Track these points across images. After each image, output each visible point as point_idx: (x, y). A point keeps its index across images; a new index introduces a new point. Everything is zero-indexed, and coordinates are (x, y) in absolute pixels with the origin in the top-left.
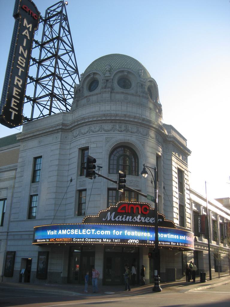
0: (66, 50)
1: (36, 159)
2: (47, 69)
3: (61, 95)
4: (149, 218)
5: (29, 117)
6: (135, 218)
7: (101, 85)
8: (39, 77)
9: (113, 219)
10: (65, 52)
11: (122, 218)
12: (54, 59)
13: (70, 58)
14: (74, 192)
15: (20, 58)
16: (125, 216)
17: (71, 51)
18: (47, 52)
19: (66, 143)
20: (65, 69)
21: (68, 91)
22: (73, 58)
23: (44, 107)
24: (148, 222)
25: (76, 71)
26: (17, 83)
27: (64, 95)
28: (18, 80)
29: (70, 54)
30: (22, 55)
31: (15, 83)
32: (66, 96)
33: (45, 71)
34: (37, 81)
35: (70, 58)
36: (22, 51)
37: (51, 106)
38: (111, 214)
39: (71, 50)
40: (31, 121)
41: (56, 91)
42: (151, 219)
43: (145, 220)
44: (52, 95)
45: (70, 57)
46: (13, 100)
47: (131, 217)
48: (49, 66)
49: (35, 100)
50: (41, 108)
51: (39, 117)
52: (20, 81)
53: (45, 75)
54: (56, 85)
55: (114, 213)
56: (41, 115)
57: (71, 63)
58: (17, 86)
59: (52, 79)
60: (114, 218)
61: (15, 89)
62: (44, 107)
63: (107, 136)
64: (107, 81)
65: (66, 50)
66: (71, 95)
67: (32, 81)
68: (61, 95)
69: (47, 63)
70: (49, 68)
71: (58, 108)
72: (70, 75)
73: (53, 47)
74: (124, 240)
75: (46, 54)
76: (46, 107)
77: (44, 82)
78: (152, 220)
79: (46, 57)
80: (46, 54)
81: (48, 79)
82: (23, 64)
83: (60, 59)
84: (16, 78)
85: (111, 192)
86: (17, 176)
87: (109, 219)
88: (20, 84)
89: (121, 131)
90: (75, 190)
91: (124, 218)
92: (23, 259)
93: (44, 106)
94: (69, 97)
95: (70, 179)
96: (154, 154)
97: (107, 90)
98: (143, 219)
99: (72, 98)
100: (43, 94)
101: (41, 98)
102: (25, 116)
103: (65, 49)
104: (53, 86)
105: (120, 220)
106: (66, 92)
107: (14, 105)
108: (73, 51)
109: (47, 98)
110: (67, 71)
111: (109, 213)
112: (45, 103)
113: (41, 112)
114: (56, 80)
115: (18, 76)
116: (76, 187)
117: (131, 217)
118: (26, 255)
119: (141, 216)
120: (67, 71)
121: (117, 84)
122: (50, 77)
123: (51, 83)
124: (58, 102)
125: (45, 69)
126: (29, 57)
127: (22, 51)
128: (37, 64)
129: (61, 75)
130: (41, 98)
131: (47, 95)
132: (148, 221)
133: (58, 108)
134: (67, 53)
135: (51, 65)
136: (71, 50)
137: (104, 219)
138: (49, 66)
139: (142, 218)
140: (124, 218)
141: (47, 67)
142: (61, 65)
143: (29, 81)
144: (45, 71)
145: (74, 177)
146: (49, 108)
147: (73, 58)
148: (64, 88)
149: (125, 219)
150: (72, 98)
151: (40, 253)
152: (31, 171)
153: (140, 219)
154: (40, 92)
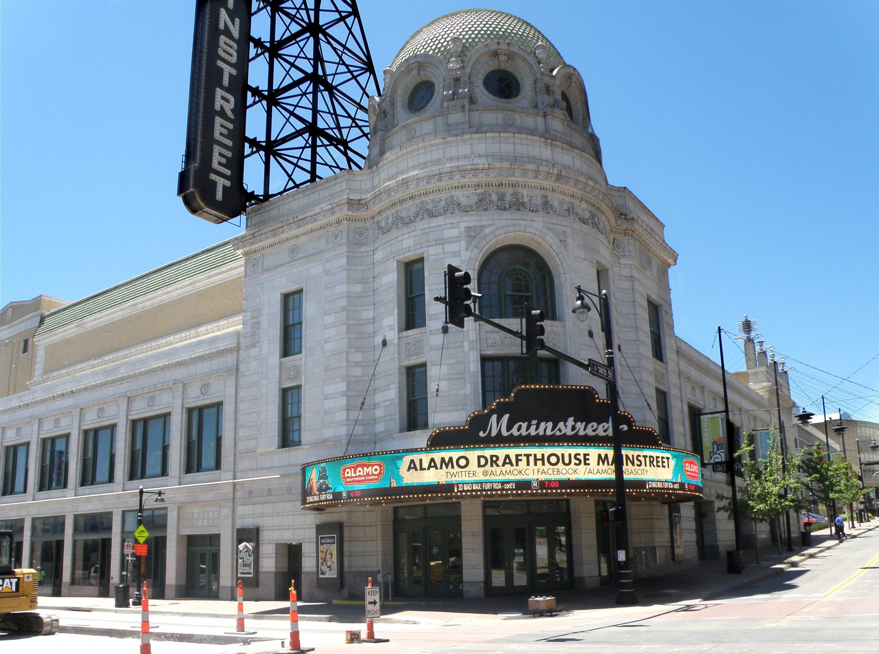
0: (340, 12)
1: (286, 297)
2: (292, 65)
3: (332, 129)
4: (595, 424)
5: (260, 191)
6: (561, 425)
7: (442, 92)
8: (275, 87)
9: (505, 433)
10: (336, 16)
11: (528, 428)
12: (308, 38)
13: (351, 32)
14: (396, 371)
15: (223, 39)
16: (534, 422)
17: (350, 14)
18: (287, 20)
19: (357, 255)
20: (337, 60)
21: (354, 120)
22: (356, 30)
23: (296, 165)
24: (594, 434)
25: (369, 67)
26: (222, 106)
27: (339, 128)
28: (223, 98)
29: (349, 21)
30: (227, 33)
31: (217, 107)
32: (345, 132)
33: (288, 73)
34: (272, 98)
35: (351, 32)
36: (225, 23)
37: (314, 162)
38: (498, 420)
39: (351, 10)
40: (267, 203)
41: (321, 124)
42: (601, 425)
43: (585, 429)
44: (312, 129)
45: (350, 29)
46: (217, 149)
47: (550, 424)
48: (297, 57)
49: (270, 148)
50: (289, 168)
51: (285, 190)
52: (227, 101)
53: (288, 81)
54: (321, 106)
55: (506, 416)
56: (291, 184)
57: (352, 45)
58: (222, 114)
59: (311, 89)
60: (509, 428)
61: (218, 120)
62: (296, 165)
63: (467, 224)
64: (457, 80)
65: (340, 12)
66: (360, 127)
67: (257, 99)
68: (332, 129)
69: (291, 50)
70: (299, 63)
71: (326, 164)
72: (355, 77)
73: (303, 7)
74: (524, 485)
75: (288, 28)
76: (301, 163)
77: (290, 99)
78: (605, 429)
79: (288, 34)
80: (288, 28)
81: (296, 91)
82: (231, 55)
83: (326, 35)
84: (219, 92)
85: (488, 365)
86: (242, 345)
87: (494, 434)
88: (229, 107)
89: (505, 209)
90: (397, 366)
91: (533, 428)
92: (278, 546)
93: (295, 161)
94: (356, 132)
95: (379, 340)
96: (592, 262)
97: (459, 103)
98: (580, 426)
99: (365, 135)
100: (288, 130)
101: (285, 140)
102: (249, 191)
103: (337, 10)
104: (315, 111)
105: (524, 432)
106: (345, 122)
107: (220, 164)
108: (355, 13)
109: (299, 142)
110: (347, 66)
111: (494, 417)
112: (296, 153)
113: (290, 176)
114: (319, 94)
115: (223, 88)
116: (399, 359)
117: (550, 424)
118: (290, 537)
119: (576, 421)
120: (347, 66)
121: (482, 87)
122: (303, 87)
123: (306, 102)
124: (332, 149)
125: (287, 66)
126: (246, 38)
127: (225, 23)
128: (267, 54)
129: (330, 79)
130: (285, 140)
131: (297, 131)
132: (594, 431)
133: (326, 164)
134: (342, 19)
135: (302, 55)
136: (351, 10)
137: (481, 434)
138: (297, 57)
139: (579, 425)
140: (533, 428)
141: (292, 60)
142: (327, 52)
143: (250, 99)
144: (288, 73)
145: (392, 335)
146: (308, 166)
147: (356, 30)
148: (340, 111)
149: (537, 429)
150: (365, 135)
151: (321, 529)
152: (279, 327)
153: (573, 428)
154: (281, 125)
